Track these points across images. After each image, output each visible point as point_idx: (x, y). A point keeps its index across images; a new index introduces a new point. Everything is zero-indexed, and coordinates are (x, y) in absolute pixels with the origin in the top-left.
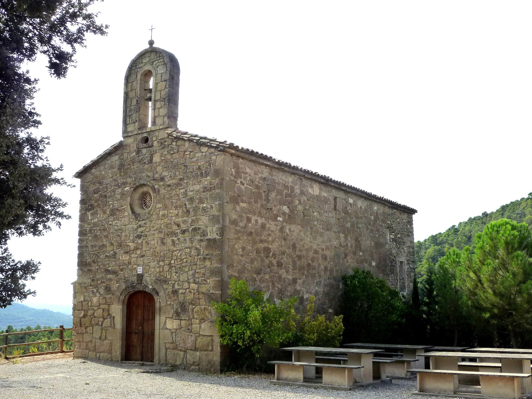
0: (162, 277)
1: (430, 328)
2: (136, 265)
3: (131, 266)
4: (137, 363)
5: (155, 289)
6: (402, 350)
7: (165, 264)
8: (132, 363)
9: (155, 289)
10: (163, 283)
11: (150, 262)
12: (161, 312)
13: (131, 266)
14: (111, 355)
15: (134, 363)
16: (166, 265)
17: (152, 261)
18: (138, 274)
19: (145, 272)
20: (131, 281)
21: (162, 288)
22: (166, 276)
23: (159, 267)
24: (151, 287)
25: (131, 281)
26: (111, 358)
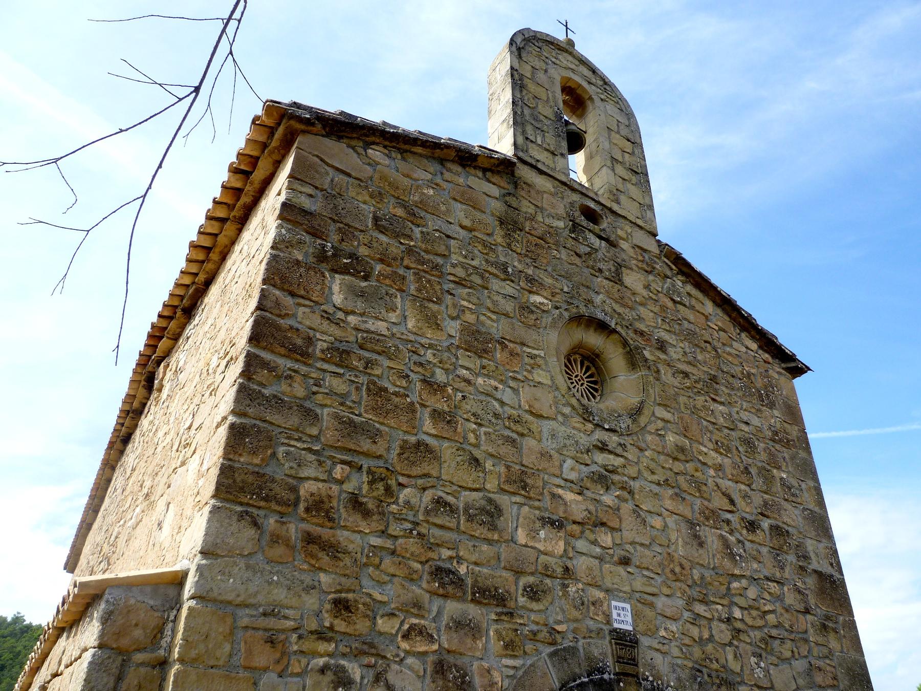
3: (580, 586)
18: (615, 630)
25: (589, 658)
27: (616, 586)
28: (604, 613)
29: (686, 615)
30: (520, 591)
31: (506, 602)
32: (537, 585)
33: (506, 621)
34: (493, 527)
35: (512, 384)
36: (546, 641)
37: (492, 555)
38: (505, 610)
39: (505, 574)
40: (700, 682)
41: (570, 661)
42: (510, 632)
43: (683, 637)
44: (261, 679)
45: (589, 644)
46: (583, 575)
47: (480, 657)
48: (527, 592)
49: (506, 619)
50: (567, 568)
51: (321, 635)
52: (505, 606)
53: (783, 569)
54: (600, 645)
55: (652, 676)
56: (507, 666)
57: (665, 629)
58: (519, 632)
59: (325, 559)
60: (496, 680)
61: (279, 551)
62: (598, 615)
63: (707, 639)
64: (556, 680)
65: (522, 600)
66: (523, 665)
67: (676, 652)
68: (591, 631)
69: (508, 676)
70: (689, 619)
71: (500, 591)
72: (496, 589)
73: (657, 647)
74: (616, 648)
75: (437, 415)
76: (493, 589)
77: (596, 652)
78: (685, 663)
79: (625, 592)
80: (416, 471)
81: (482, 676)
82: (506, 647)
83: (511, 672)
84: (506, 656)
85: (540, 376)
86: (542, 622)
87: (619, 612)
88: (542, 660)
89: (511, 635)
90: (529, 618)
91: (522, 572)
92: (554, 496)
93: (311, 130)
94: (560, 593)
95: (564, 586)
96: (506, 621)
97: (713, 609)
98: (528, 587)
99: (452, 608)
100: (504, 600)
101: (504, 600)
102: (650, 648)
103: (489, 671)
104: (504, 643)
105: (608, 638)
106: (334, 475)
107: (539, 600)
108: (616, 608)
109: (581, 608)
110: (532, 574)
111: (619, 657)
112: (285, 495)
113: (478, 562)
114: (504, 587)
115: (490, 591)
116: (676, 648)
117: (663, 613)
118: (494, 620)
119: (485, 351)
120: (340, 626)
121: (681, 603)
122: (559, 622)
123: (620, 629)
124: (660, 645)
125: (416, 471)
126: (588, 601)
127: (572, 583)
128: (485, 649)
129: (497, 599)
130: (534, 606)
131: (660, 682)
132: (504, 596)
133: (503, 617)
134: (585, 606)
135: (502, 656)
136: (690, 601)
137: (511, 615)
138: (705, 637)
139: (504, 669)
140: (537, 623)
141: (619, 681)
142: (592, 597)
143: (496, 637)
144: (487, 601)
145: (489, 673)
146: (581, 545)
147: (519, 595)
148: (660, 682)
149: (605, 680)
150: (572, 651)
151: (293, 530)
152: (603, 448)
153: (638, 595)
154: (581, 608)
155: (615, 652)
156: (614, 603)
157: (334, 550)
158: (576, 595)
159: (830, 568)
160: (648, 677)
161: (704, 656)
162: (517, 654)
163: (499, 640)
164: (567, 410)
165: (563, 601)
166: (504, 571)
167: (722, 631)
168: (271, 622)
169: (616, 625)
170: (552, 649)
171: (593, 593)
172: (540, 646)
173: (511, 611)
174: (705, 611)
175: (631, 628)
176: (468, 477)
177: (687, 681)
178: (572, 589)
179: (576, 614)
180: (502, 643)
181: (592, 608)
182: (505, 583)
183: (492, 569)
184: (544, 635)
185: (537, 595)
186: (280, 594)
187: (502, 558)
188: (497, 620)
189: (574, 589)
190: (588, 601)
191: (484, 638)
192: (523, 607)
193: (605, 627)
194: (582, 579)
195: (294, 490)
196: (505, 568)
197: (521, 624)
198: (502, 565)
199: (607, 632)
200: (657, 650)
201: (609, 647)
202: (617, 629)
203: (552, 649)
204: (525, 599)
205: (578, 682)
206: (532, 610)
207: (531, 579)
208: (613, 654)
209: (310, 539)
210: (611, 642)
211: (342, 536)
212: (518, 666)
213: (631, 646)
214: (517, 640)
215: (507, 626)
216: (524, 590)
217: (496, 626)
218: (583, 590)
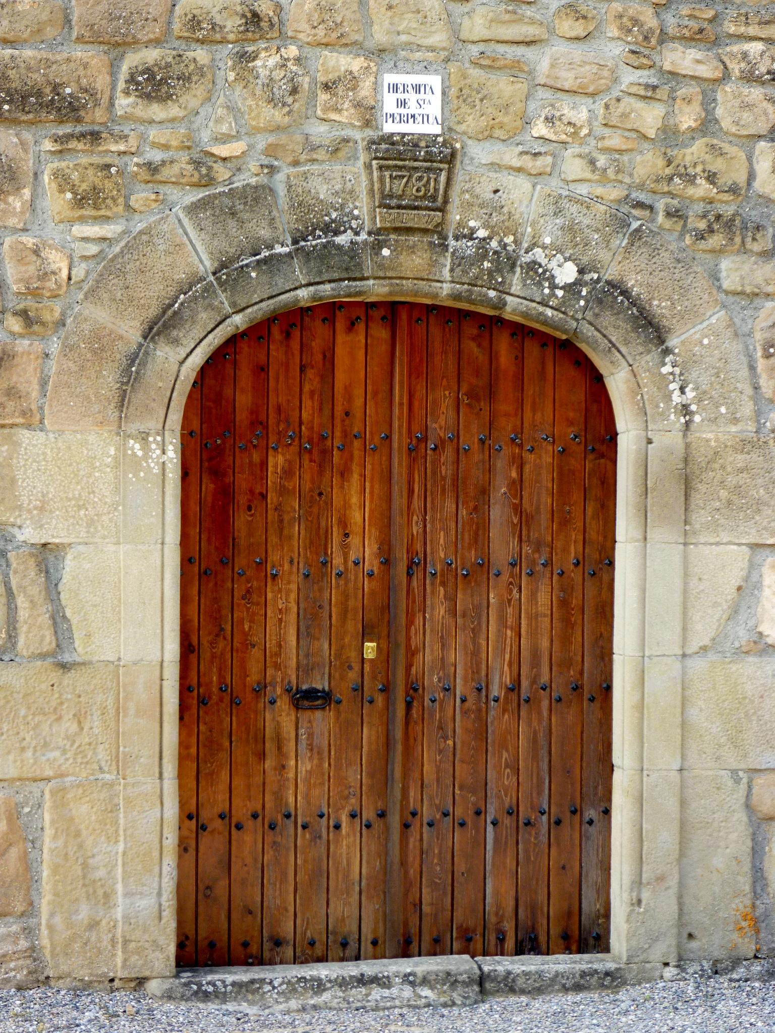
0: (703, 188)
1: (687, 1)
2: (355, 47)
3: (292, 51)
4: (409, 979)
5: (625, 293)
6: (403, 371)
7: (736, 68)
8: (343, 983)
9: (617, 287)
10: (716, 240)
11: (531, 31)
12: (697, 499)
13: (292, 51)
14: (29, 932)
15: (362, 981)
16: (750, 78)
17: (569, 27)
18: (388, 139)
19: (472, 123)
20: (299, 205)
21: (702, 283)
22: (741, 178)
23: (662, 93)
24: (567, 274)
25: (299, 205)
26: (33, 952)
27: (404, 38)
28: (358, 105)
29: (630, 77)
30: (121, 85)
31: (82, 113)
32: (168, 65)
33: (83, 151)
36: (184, 181)
37: (44, 17)
38: (79, 129)
39: (80, 53)
40: (637, 230)
41: (246, 216)
42: (90, 172)
43: (607, 132)
44: (351, 977)
45: (305, 176)
46: (304, 26)
47: (21, 226)
48: (138, 84)
49: (80, 146)
50: (255, 15)
52: (79, 120)
54: (338, 175)
55: (486, 226)
56: (85, 239)
57: (549, 120)
58: (113, 170)
60: (54, 267)
62: (339, 111)
63: (691, 130)
64: (204, 257)
65: (124, 103)
66: (124, 232)
67: (574, 167)
68: (314, 149)
69: (84, 258)
70: (634, 90)
71: (68, 91)
72: (56, 88)
73: (516, 163)
74: (382, 180)
76: (48, 90)
78: (599, 191)
79: (432, 49)
81: (21, 261)
82: (80, 201)
83: (93, 249)
84: (82, 220)
86: (174, 143)
87: (401, 96)
88: (172, 220)
89: (94, 177)
90: (143, 137)
91: (125, 44)
94: (232, 76)
95: (244, 58)
96: (83, 151)
97: (732, 55)
98: (143, 73)
100: (75, 110)
101: (75, 110)
102: (495, 166)
103: (36, 252)
104: (75, 194)
105: (363, 157)
107: (169, 97)
108: (395, 88)
109: (290, 100)
110: (157, 42)
111: (384, 196)
113: (10, 36)
114: (78, 81)
115: (39, 94)
116: (578, 161)
117: (552, 83)
118: (50, 151)
122: (224, 139)
123: (403, 135)
124: (527, 158)
126: (314, 81)
127: (266, 49)
128: (32, 205)
129: (59, 109)
130: (157, 111)
131: (509, 239)
132: (78, 99)
133: (73, 144)
134: (302, 96)
135: (71, 222)
137: (95, 136)
138: (684, 127)
139: (77, 245)
140: (166, 147)
141: (377, 246)
142: (326, 72)
143: (54, 185)
144: (31, 116)
145: (38, 256)
147: (119, 94)
148: (509, 239)
149: (339, 247)
153: (475, 50)
154: (290, 100)
155: (377, 186)
156: (390, 78)
158: (279, 74)
160: (473, 231)
161: (668, 171)
162: (109, 213)
163: (62, 191)
165: (238, 89)
166: (79, 47)
167: (747, 106)
169: (389, 128)
170: (201, 194)
171: (332, 63)
172: (172, 193)
173: (97, 128)
174: (698, 62)
175: (436, 129)
177: (597, 230)
179: (278, 116)
180: (69, 195)
181: (323, 97)
182: (81, 72)
183: (51, 48)
184: (183, 163)
185: (164, 89)
187: (75, 19)
188: (61, 152)
189: (273, 61)
190: (314, 81)
191: (27, 193)
192: (127, 117)
193: (357, 135)
194: (301, 36)
196: (80, 39)
197: (121, 154)
198: (74, 35)
199: (361, 145)
200: (519, 170)
201: (364, 178)
202: (392, 134)
203: (201, 196)
204: (131, 99)
205: (265, 253)
206: (151, 122)
207: (151, 55)
208: (371, 191)
210: (368, 167)
212: (109, 235)
213: (428, 169)
214: (108, 185)
215: (84, 160)
216: (132, 80)
217: (56, 165)
218: (298, 60)
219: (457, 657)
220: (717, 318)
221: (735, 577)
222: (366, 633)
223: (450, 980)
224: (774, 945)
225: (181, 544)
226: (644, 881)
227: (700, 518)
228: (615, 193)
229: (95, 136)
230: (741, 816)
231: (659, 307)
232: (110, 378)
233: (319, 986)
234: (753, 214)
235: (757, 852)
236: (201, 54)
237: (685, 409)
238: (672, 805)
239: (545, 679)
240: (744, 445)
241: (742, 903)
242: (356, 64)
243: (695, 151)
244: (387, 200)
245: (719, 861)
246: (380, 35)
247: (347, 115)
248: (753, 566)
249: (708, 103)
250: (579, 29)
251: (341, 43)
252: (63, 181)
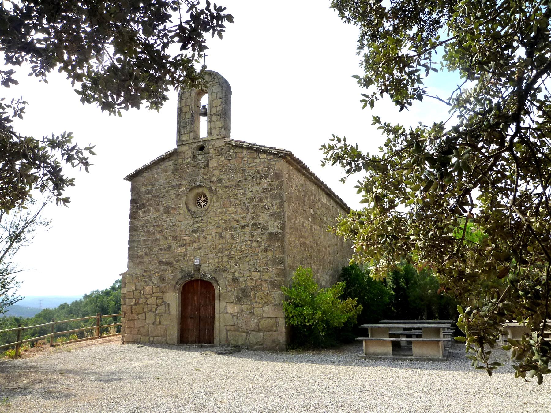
4: (196, 345)
16: (226, 256)
19: (202, 262)
20: (188, 271)
24: (209, 276)
34: (169, 251)
35: (175, 217)
51: (143, 276)
53: (200, 199)
59: (143, 265)
61: (137, 265)
67: (210, 266)
75: (159, 232)
77: (190, 270)
80: (156, 244)
85: (181, 211)
92: (183, 239)
93: (407, 337)
99: (162, 267)
106: (533, 371)
112: (136, 256)
119: (168, 212)
120: (145, 274)
121: (214, 254)
125: (156, 244)
130: (177, 264)
136: (217, 254)
146: (189, 248)
150: (184, 271)
151: (138, 261)
152: (197, 222)
157: (143, 263)
159: (278, 229)
164: (187, 217)
168: (137, 276)
176: (165, 242)
178: (186, 258)
179: (186, 263)
186: (137, 271)
195: (138, 255)
207: (177, 259)
209: (140, 262)
211: (145, 260)
219: (204, 313)
220: (223, 280)
221: (224, 305)
222: (196, 311)
223: (199, 346)
224: (128, 1)
225: (181, 303)
226: (221, 313)
227: (221, 300)
228: (213, 268)
229: (173, 266)
230: (225, 330)
231: (217, 279)
232: (173, 288)
233: (188, 345)
234: (226, 269)
235: (227, 334)
236: (181, 258)
237: (219, 289)
238: (218, 328)
239: (449, 325)
240: (225, 292)
241: (225, 339)
242: (193, 258)
243: (221, 264)
244: (194, 270)
245: (223, 335)
246: (195, 255)
247: (192, 263)
248: (226, 304)
249: (222, 258)
250: (202, 199)
251: (191, 256)
252: (170, 271)
